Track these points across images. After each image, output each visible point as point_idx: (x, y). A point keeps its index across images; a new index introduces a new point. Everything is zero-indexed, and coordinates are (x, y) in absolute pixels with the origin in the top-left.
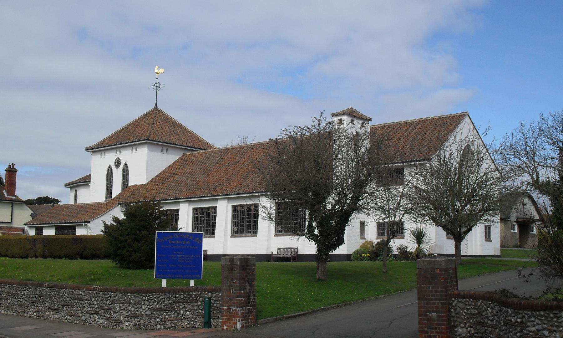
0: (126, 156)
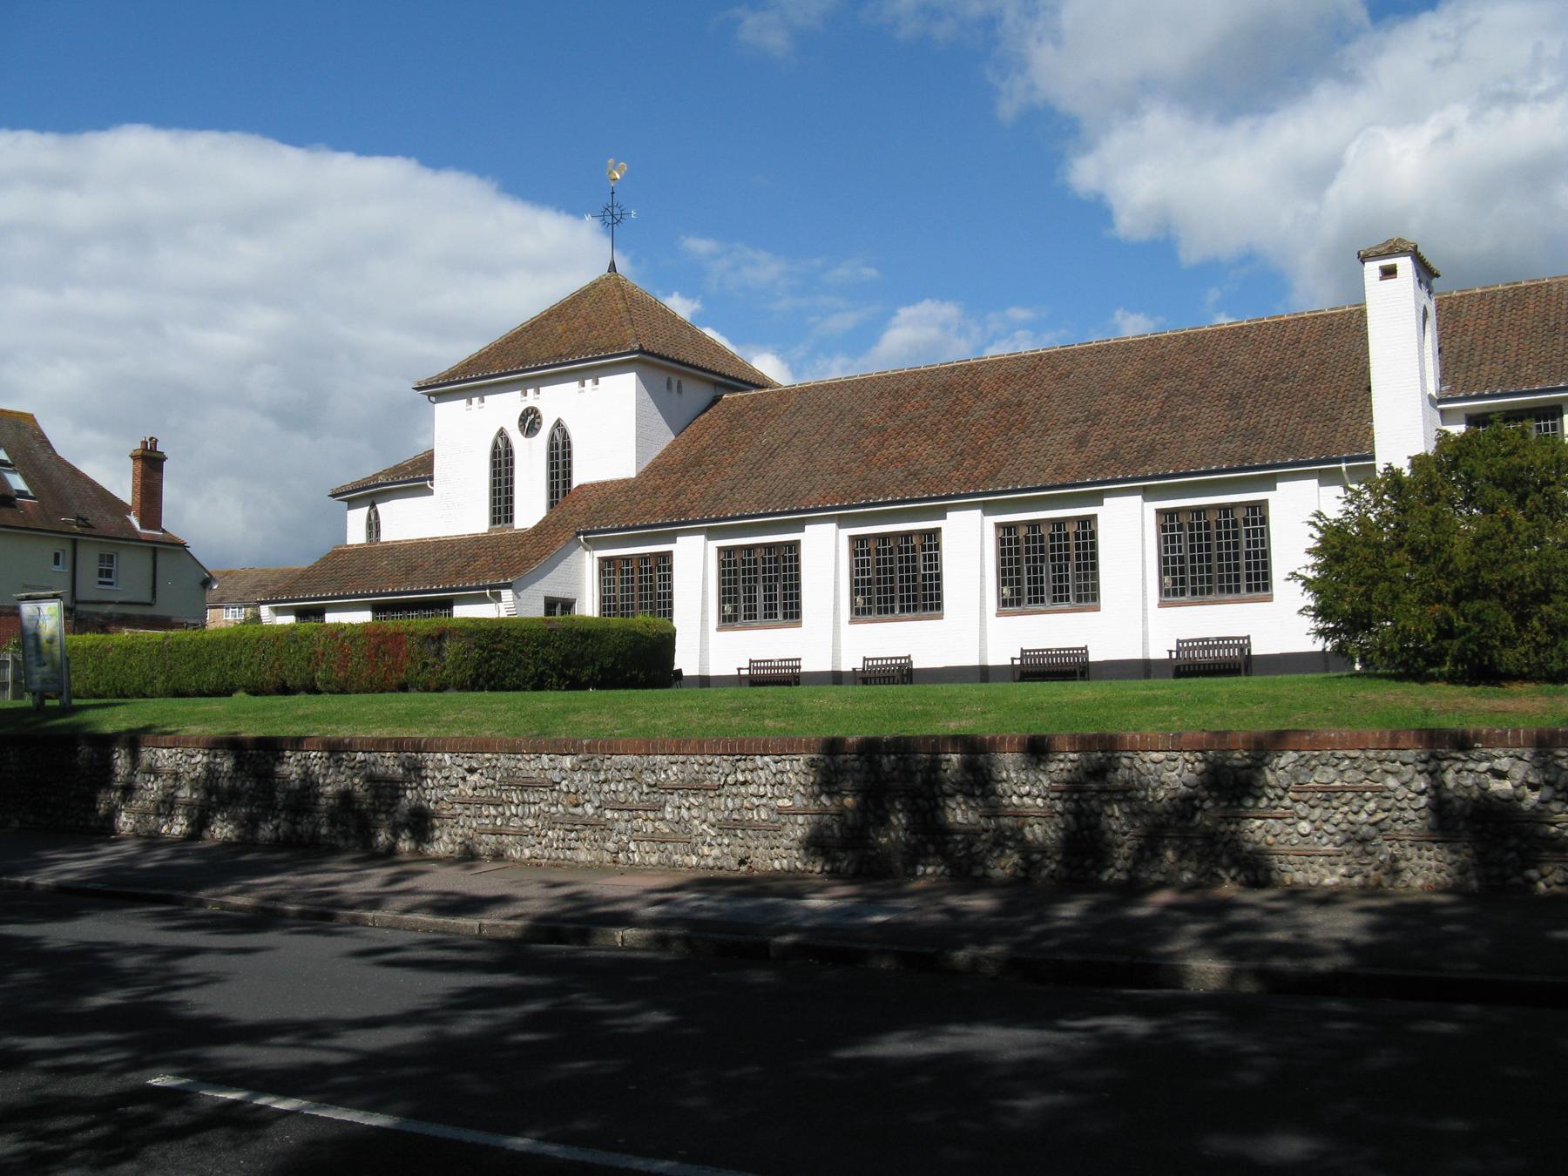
0: (558, 401)
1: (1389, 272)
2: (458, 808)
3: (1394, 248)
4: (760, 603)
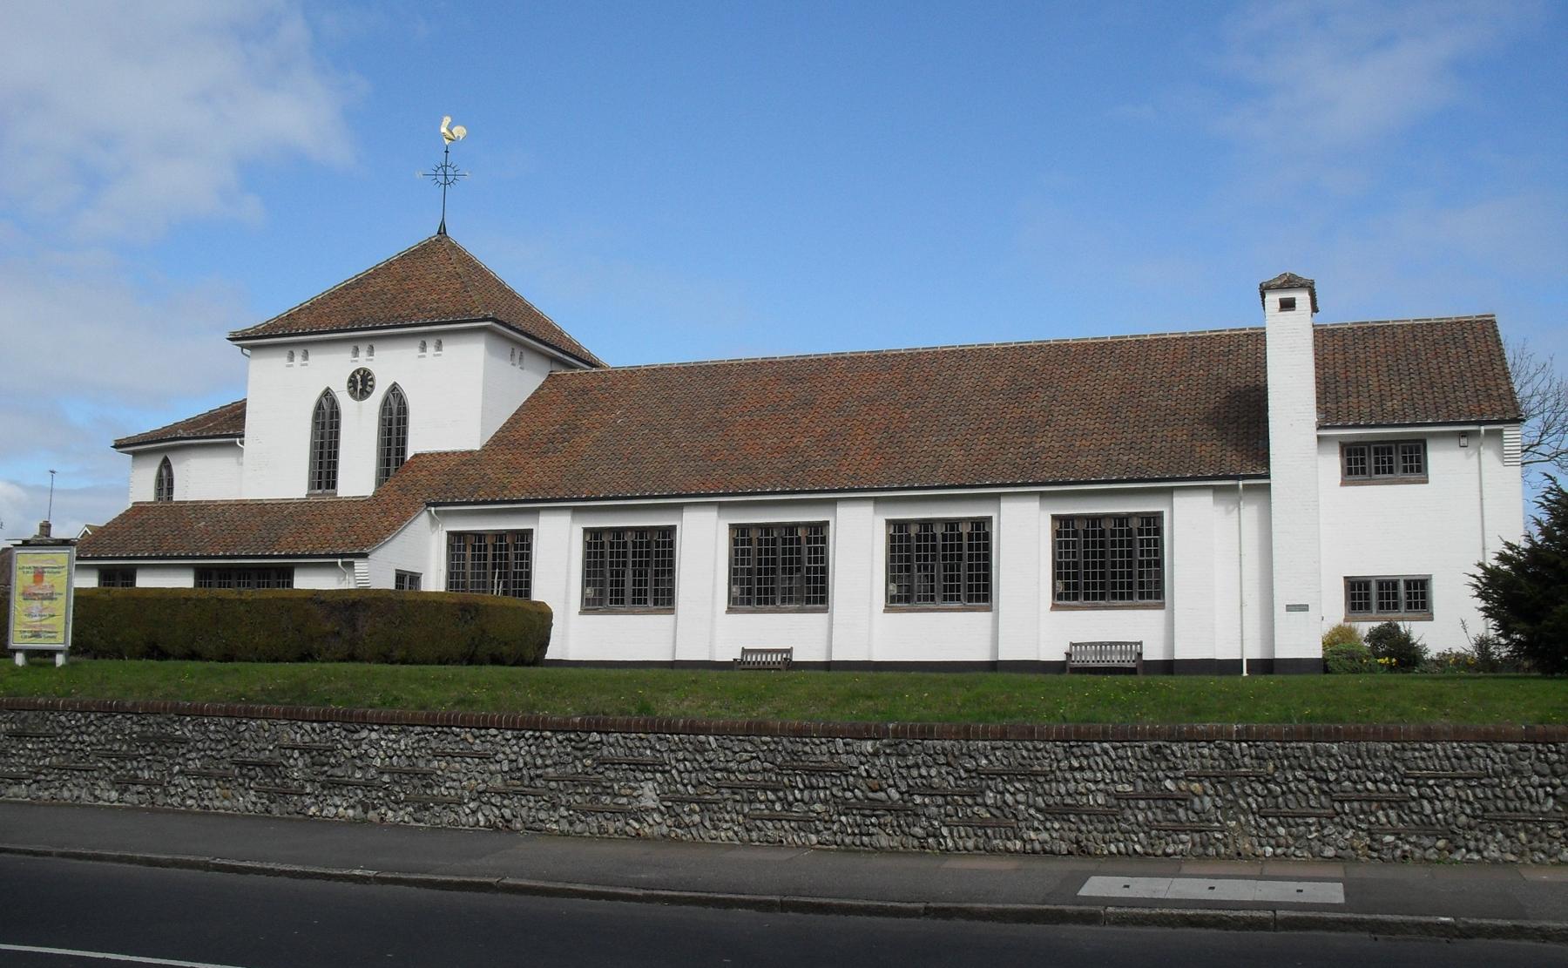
0: (393, 364)
1: (1287, 305)
2: (726, 793)
3: (1290, 282)
4: (629, 587)
